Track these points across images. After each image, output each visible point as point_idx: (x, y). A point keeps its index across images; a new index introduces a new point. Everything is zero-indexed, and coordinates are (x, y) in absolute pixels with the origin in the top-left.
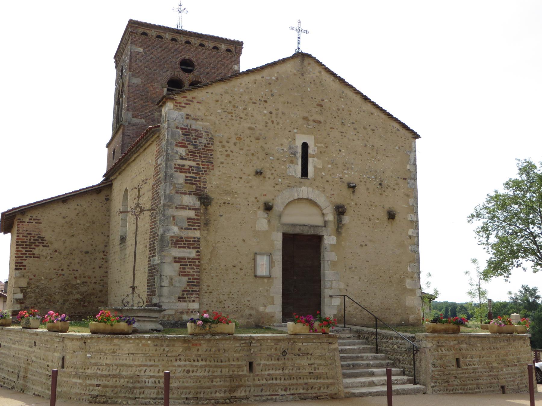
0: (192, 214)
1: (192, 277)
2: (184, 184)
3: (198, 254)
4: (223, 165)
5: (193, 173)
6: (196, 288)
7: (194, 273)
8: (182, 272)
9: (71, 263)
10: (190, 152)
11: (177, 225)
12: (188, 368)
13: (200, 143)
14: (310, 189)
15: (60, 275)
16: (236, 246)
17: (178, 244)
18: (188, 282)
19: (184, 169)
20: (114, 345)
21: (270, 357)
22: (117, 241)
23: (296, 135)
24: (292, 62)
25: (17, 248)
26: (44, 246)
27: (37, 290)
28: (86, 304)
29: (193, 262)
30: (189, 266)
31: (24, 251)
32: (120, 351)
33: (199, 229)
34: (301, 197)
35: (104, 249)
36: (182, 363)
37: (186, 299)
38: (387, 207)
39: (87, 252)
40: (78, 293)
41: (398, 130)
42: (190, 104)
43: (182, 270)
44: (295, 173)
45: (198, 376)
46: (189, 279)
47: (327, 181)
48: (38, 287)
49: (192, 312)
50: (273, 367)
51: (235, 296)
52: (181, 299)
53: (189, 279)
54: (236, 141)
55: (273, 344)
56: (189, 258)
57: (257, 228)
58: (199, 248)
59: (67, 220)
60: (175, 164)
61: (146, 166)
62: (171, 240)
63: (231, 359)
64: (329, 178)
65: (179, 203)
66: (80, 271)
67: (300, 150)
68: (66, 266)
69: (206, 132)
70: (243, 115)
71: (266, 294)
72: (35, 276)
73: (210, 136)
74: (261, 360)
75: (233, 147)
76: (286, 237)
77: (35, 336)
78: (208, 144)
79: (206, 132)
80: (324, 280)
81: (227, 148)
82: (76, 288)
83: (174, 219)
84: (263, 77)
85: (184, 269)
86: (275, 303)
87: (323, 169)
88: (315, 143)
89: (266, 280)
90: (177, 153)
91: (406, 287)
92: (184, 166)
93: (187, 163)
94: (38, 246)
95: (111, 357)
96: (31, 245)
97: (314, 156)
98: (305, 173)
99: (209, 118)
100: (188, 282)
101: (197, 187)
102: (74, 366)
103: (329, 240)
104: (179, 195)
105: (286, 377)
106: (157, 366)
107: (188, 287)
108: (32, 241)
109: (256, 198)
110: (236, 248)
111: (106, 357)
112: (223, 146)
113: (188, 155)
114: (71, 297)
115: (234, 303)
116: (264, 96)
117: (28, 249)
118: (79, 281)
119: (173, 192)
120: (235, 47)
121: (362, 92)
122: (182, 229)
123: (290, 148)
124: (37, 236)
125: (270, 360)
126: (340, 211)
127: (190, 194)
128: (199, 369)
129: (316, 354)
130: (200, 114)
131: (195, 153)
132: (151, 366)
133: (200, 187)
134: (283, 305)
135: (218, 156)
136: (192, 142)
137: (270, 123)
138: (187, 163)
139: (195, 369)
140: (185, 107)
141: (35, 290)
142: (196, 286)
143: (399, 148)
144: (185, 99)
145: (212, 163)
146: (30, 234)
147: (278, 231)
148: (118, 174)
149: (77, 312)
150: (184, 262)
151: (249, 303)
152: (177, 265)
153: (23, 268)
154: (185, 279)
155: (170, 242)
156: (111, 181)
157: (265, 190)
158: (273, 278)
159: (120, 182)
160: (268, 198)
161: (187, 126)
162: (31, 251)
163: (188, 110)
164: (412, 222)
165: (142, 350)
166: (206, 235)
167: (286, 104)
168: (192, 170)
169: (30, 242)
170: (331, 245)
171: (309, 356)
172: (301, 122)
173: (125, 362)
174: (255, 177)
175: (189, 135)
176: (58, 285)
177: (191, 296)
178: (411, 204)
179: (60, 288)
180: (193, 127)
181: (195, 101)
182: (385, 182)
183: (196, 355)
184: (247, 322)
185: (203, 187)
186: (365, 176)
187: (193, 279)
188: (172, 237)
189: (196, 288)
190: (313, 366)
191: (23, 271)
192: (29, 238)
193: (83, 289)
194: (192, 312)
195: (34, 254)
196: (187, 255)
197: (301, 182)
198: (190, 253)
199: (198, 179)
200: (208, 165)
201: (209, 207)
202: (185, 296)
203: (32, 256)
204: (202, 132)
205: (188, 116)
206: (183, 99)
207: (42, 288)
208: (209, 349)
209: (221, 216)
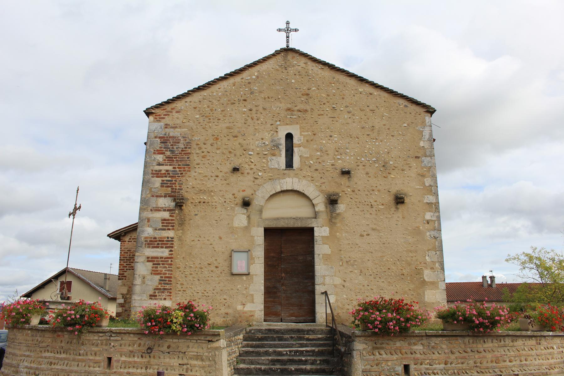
0: (166, 215)
1: (164, 276)
2: (160, 187)
3: (171, 253)
4: (199, 166)
5: (169, 177)
6: (168, 287)
7: (166, 272)
8: (154, 271)
10: (166, 158)
11: (151, 227)
12: (51, 360)
13: (177, 148)
14: (296, 180)
16: (211, 244)
17: (151, 244)
19: (161, 174)
21: (132, 353)
23: (279, 127)
25: (120, 262)
29: (166, 261)
30: (161, 265)
31: (125, 264)
33: (173, 229)
34: (285, 189)
38: (394, 190)
41: (406, 106)
42: (169, 115)
43: (154, 269)
45: (57, 369)
46: (162, 277)
47: (317, 170)
50: (134, 365)
52: (152, 297)
53: (162, 277)
54: (213, 141)
55: (136, 339)
60: (152, 171)
62: (146, 241)
63: (89, 353)
64: (319, 167)
65: (154, 206)
67: (283, 141)
69: (184, 137)
70: (221, 116)
71: (245, 292)
74: (121, 356)
75: (209, 148)
78: (186, 148)
79: (184, 137)
81: (204, 150)
84: (243, 78)
85: (157, 267)
86: (255, 301)
87: (311, 157)
88: (301, 132)
91: (424, 280)
92: (161, 171)
93: (164, 168)
97: (299, 146)
98: (289, 164)
99: (188, 124)
103: (321, 232)
104: (155, 198)
107: (160, 286)
108: (131, 256)
109: (233, 195)
110: (212, 246)
112: (200, 148)
113: (165, 160)
115: (209, 301)
116: (243, 96)
117: (128, 263)
119: (149, 196)
121: (356, 73)
122: (156, 230)
125: (132, 356)
126: (332, 201)
127: (165, 197)
128: (60, 361)
129: (190, 353)
130: (178, 122)
131: (172, 158)
133: (176, 189)
134: (265, 302)
135: (195, 159)
136: (169, 148)
137: (250, 120)
138: (164, 168)
139: (57, 361)
140: (164, 118)
142: (167, 284)
143: (408, 125)
144: (164, 111)
145: (189, 165)
147: (258, 226)
150: (157, 261)
152: (150, 264)
154: (157, 277)
155: (145, 243)
157: (242, 186)
158: (253, 275)
160: (247, 193)
163: (167, 120)
164: (430, 204)
167: (267, 99)
168: (169, 174)
171: (181, 355)
174: (232, 174)
175: (167, 143)
177: (163, 294)
178: (427, 184)
180: (171, 135)
181: (174, 111)
182: (391, 163)
183: (59, 348)
184: (223, 321)
185: (179, 189)
186: (363, 159)
187: (165, 277)
188: (146, 238)
189: (168, 287)
190: (185, 367)
191: (124, 280)
192: (129, 254)
196: (160, 255)
197: (284, 174)
198: (162, 252)
199: (174, 182)
200: (184, 168)
202: (157, 294)
205: (167, 126)
209: (196, 215)
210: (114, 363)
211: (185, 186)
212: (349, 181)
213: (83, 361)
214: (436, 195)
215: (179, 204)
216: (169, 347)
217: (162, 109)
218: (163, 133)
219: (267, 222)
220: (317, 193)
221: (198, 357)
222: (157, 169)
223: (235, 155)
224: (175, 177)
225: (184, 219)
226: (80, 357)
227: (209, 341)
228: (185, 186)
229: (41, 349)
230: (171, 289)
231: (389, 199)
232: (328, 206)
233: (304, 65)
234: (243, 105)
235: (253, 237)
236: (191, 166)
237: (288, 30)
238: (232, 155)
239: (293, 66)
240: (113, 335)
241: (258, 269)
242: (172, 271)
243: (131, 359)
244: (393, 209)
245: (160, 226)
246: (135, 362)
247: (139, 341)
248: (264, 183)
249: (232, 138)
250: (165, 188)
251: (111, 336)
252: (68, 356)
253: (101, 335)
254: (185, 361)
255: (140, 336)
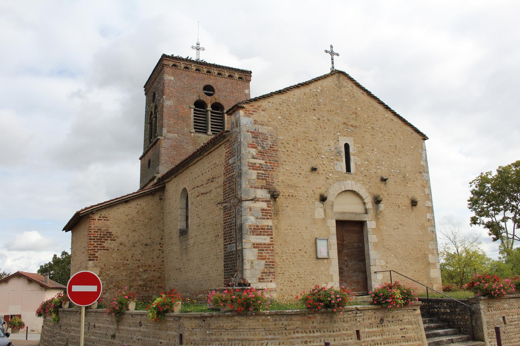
0: (264, 205)
5: (263, 170)
6: (272, 270)
8: (260, 256)
9: (134, 254)
10: (259, 152)
11: (253, 215)
14: (353, 182)
15: (126, 264)
17: (255, 232)
18: (266, 265)
19: (256, 167)
20: (234, 322)
21: (371, 325)
22: (175, 234)
23: (339, 137)
24: (330, 79)
26: (111, 240)
27: (107, 278)
28: (148, 289)
31: (96, 244)
32: (241, 327)
33: (271, 219)
35: (160, 242)
36: (300, 335)
37: (265, 280)
39: (147, 245)
40: (141, 280)
43: (260, 254)
44: (342, 168)
48: (108, 275)
49: (270, 291)
50: (374, 334)
51: (303, 276)
53: (266, 262)
55: (373, 313)
56: (265, 244)
57: (316, 216)
58: (272, 235)
59: (130, 217)
60: (248, 163)
61: (213, 167)
62: (250, 229)
63: (341, 329)
64: (366, 173)
66: (142, 261)
67: (343, 150)
68: (130, 256)
69: (271, 135)
71: (327, 273)
72: (105, 266)
73: (274, 139)
76: (339, 223)
77: (139, 317)
79: (271, 135)
80: (369, 259)
81: (288, 149)
82: (139, 276)
83: (251, 210)
85: (262, 253)
86: (334, 280)
89: (326, 261)
90: (249, 153)
92: (255, 164)
93: (258, 162)
94: (107, 240)
95: (231, 333)
96: (101, 239)
98: (348, 169)
99: (273, 123)
100: (266, 265)
101: (267, 182)
102: (193, 342)
103: (371, 225)
105: (385, 342)
106: (278, 339)
108: (102, 235)
111: (226, 333)
113: (258, 154)
114: (135, 283)
116: (313, 105)
117: (99, 243)
118: (141, 270)
119: (248, 186)
120: (245, 76)
121: (384, 102)
122: (257, 218)
123: (336, 148)
124: (106, 232)
126: (377, 201)
127: (262, 188)
130: (265, 120)
131: (263, 153)
132: (272, 339)
135: (282, 156)
137: (319, 128)
138: (258, 162)
139: (312, 340)
140: (253, 114)
141: (106, 278)
142: (272, 268)
144: (252, 107)
146: (101, 230)
147: (332, 218)
148: (173, 177)
149: (141, 295)
151: (314, 281)
152: (256, 250)
153: (96, 259)
154: (263, 262)
156: (165, 183)
157: (318, 183)
159: (176, 183)
160: (322, 191)
161: (255, 130)
162: (101, 244)
163: (256, 116)
165: (262, 325)
166: (276, 224)
167: (330, 112)
168: (262, 167)
169: (100, 237)
170: (372, 229)
171: (400, 322)
172: (342, 126)
173: (246, 337)
174: (310, 173)
175: (257, 138)
176: (124, 273)
177: (269, 277)
179: (126, 276)
180: (260, 131)
181: (260, 109)
188: (250, 226)
189: (272, 270)
190: (403, 330)
191: (95, 261)
192: (99, 233)
193: (145, 276)
194: (270, 291)
195: (104, 247)
196: (263, 242)
198: (265, 239)
200: (274, 163)
201: (277, 199)
202: (264, 277)
203: (102, 248)
204: (267, 135)
205: (256, 122)
206: (251, 107)
207: (111, 276)
208: (322, 321)
210: (362, 335)
211: (277, 180)
212: (386, 186)
213: (338, 336)
214: (431, 200)
215: (274, 196)
216: (392, 317)
217: (250, 105)
218: (254, 128)
219: (337, 216)
220: (367, 194)
221: (410, 323)
222: (253, 162)
223: (312, 157)
224: (268, 171)
225: (278, 209)
226: (335, 333)
227: (414, 310)
228: (277, 180)
229: (290, 331)
230: (274, 272)
231: (408, 202)
232: (375, 205)
233: (351, 88)
234: (313, 114)
235: (328, 227)
236: (279, 162)
237: (332, 53)
238: (310, 157)
239: (344, 87)
240: (358, 312)
241: (334, 254)
242: (273, 256)
243: (371, 330)
244: (410, 210)
245: (260, 215)
246: (375, 332)
247: (375, 315)
248: (334, 183)
249: (308, 141)
250: (260, 180)
251: (357, 313)
252: (323, 334)
253: (349, 313)
254: (403, 327)
255: (375, 311)
